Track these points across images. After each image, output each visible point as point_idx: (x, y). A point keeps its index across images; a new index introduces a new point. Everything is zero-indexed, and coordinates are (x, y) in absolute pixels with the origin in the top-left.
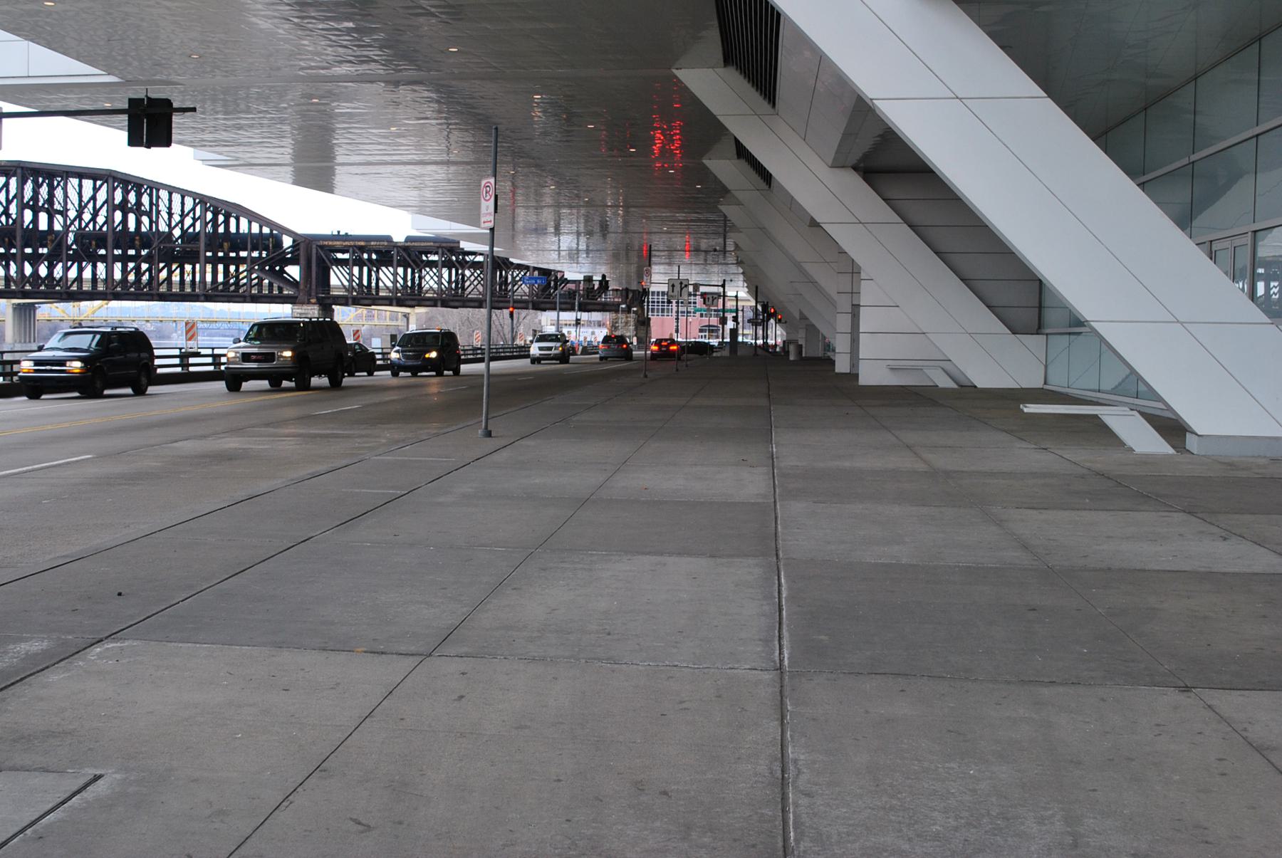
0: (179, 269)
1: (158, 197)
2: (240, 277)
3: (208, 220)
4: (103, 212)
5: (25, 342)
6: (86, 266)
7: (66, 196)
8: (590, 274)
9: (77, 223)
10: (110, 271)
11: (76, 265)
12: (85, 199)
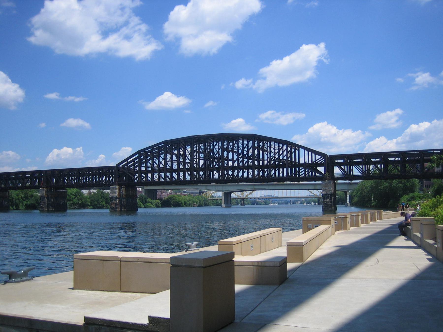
0: (278, 170)
1: (270, 145)
2: (303, 172)
3: (289, 150)
4: (251, 151)
5: (228, 204)
6: (245, 171)
7: (238, 146)
8: (319, 206)
9: (242, 155)
10: (253, 172)
11: (242, 171)
12: (280, 148)
